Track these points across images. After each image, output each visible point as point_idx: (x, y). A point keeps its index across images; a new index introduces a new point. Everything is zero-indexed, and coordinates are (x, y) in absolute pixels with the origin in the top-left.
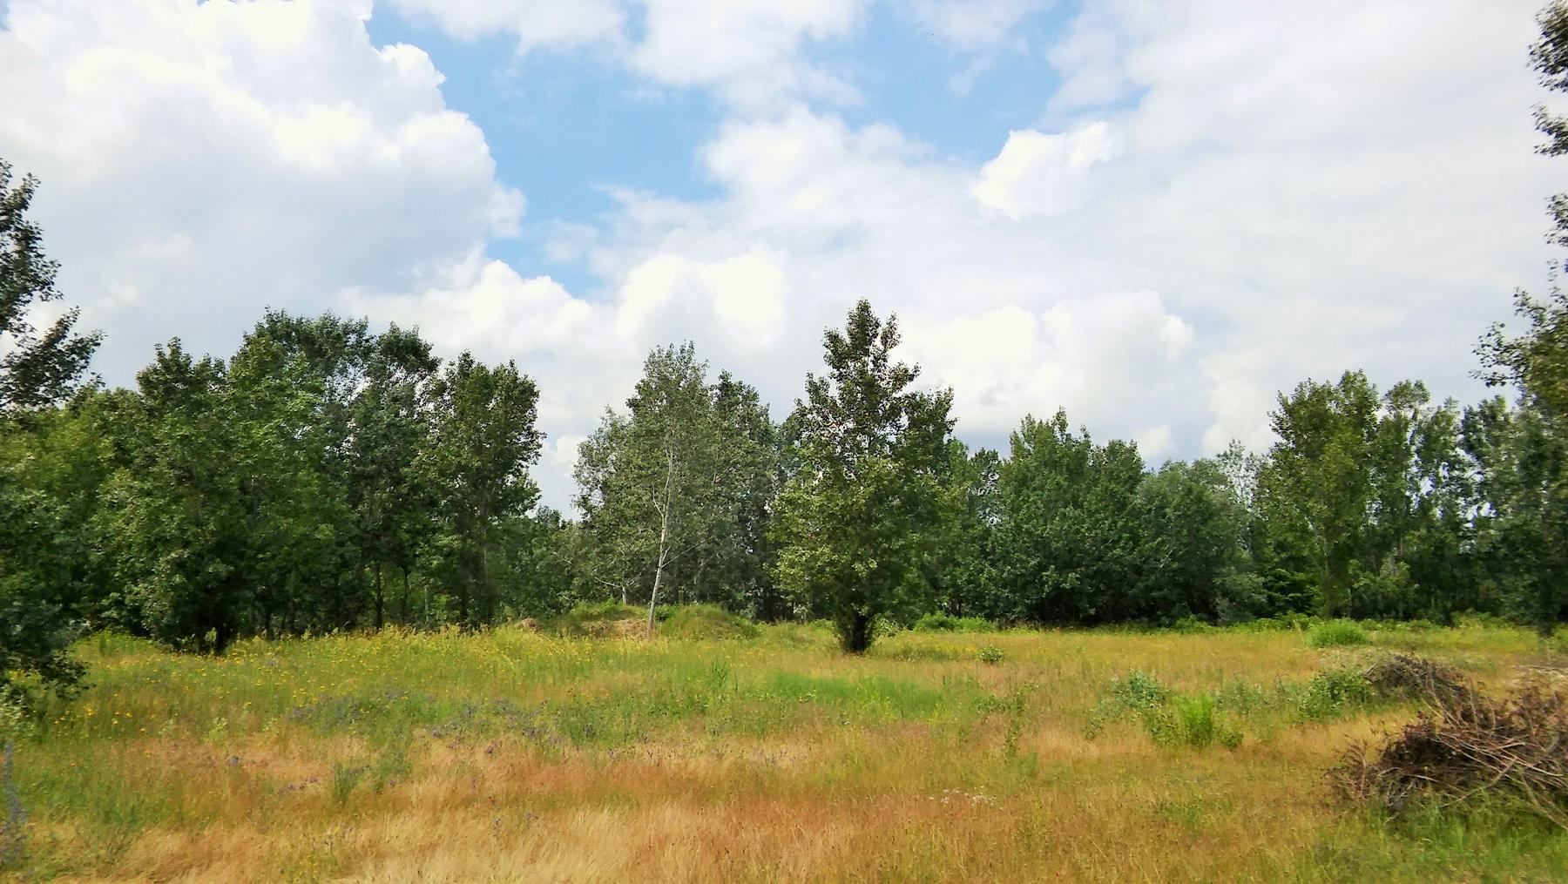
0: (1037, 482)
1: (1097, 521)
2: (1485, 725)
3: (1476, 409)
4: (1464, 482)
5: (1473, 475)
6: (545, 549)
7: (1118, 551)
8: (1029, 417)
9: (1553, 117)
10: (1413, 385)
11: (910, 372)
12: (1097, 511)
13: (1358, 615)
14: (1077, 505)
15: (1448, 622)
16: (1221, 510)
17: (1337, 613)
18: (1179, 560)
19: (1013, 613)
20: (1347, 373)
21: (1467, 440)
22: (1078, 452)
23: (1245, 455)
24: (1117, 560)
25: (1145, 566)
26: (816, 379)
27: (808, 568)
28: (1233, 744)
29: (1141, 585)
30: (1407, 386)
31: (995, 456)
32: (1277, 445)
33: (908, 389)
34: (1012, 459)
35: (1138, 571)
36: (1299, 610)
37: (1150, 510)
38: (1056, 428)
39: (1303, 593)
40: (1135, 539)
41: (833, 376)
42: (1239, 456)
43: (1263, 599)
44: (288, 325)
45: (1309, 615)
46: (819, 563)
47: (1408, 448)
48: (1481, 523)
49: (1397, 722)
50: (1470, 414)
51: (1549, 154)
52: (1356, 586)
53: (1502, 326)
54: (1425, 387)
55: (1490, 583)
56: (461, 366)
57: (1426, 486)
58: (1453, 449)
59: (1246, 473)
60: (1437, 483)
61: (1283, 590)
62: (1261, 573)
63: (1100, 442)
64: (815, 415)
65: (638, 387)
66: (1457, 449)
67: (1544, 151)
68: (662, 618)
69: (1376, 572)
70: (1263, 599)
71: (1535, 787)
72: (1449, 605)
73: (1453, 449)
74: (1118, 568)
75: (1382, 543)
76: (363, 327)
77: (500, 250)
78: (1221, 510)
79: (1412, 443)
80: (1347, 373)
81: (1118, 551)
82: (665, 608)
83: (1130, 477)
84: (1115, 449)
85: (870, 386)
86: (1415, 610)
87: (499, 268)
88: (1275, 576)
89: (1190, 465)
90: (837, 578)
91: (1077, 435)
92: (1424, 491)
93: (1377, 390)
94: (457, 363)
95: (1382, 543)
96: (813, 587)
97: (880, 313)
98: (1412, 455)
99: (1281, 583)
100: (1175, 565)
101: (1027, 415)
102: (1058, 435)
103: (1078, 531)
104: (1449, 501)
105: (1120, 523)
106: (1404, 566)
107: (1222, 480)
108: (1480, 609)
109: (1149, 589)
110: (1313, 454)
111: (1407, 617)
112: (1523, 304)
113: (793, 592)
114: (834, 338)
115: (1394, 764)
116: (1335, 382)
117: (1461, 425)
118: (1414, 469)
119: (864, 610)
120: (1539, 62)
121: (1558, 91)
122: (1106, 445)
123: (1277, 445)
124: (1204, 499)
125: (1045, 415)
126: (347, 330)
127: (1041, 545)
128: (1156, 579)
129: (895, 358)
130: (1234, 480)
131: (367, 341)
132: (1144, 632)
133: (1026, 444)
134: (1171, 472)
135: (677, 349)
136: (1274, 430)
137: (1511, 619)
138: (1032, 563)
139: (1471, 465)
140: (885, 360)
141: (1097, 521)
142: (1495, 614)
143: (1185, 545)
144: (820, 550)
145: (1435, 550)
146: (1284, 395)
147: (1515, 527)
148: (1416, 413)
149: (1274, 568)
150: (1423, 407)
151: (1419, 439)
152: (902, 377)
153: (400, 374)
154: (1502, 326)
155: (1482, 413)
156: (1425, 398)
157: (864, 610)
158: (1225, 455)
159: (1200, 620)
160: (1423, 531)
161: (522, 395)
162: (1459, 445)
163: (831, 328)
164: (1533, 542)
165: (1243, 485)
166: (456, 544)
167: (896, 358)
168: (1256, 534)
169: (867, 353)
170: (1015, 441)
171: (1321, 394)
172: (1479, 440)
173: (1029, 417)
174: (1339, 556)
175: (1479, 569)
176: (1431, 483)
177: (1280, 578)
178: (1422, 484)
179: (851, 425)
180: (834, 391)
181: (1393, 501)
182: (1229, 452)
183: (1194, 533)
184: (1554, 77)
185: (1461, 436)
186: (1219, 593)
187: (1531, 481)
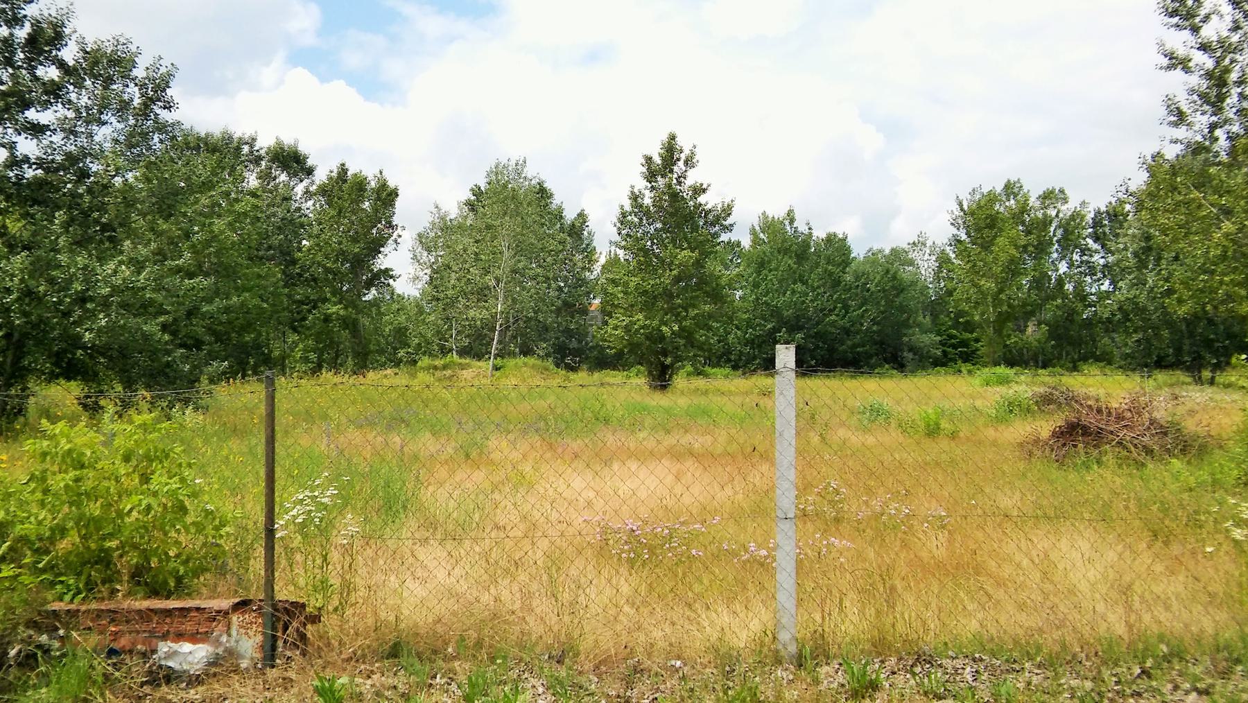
0: (773, 265)
1: (818, 294)
2: (1109, 414)
3: (1103, 209)
4: (1091, 264)
5: (1098, 259)
6: (392, 315)
7: (833, 317)
8: (764, 213)
9: (1168, 47)
10: (1057, 191)
11: (704, 186)
12: (819, 287)
13: (1011, 363)
14: (804, 283)
15: (1075, 369)
16: (910, 286)
17: (996, 364)
18: (878, 324)
19: (753, 365)
20: (1009, 181)
21: (1095, 233)
22: (804, 241)
23: (929, 243)
24: (833, 323)
25: (852, 329)
26: (636, 191)
27: (627, 329)
28: (953, 436)
29: (849, 343)
30: (1052, 192)
31: (739, 244)
32: (954, 236)
33: (702, 199)
34: (751, 246)
35: (847, 332)
36: (965, 361)
37: (858, 286)
38: (787, 222)
39: (968, 348)
40: (846, 308)
41: (646, 188)
42: (924, 244)
43: (939, 353)
44: (199, 139)
45: (973, 365)
46: (636, 327)
47: (1051, 239)
48: (1103, 296)
49: (1058, 420)
50: (1098, 213)
51: (1164, 70)
52: (1008, 343)
53: (1129, 179)
54: (1066, 192)
55: (1106, 340)
56: (339, 173)
57: (1063, 267)
58: (1084, 239)
59: (929, 258)
60: (1071, 265)
61: (954, 347)
62: (939, 334)
63: (820, 233)
64: (633, 217)
65: (472, 190)
66: (1087, 239)
67: (1161, 68)
68: (497, 368)
69: (1023, 331)
70: (939, 353)
71: (1135, 446)
72: (1076, 357)
73: (1084, 239)
74: (833, 330)
75: (1027, 312)
76: (254, 140)
77: (301, 57)
78: (910, 286)
79: (1054, 236)
80: (1009, 181)
81: (833, 317)
82: (499, 361)
83: (843, 260)
84: (830, 239)
85: (675, 196)
86: (1050, 360)
87: (301, 73)
88: (948, 336)
89: (887, 252)
90: (647, 338)
91: (803, 228)
92: (1061, 272)
93: (1030, 194)
94: (336, 171)
95: (1027, 312)
96: (630, 344)
97: (684, 143)
98: (1054, 245)
99: (953, 341)
100: (875, 328)
101: (762, 211)
102: (788, 228)
103: (803, 302)
104: (1079, 279)
105: (835, 296)
106: (1044, 328)
107: (911, 263)
108: (1098, 359)
109: (855, 346)
110: (986, 246)
111: (1044, 367)
112: (1144, 163)
113: (615, 348)
114: (649, 160)
115: (1058, 437)
116: (999, 188)
117: (1091, 221)
118: (1055, 255)
119: (669, 361)
120: (1162, 10)
121: (1173, 29)
122: (824, 236)
123: (954, 236)
124: (898, 277)
125: (777, 211)
126: (241, 142)
127: (776, 313)
128: (861, 338)
129: (693, 178)
130: (920, 262)
131: (258, 151)
132: (852, 377)
133: (762, 235)
134: (873, 257)
135: (513, 163)
136: (952, 224)
137: (1120, 367)
138: (769, 326)
139: (1096, 252)
140: (685, 178)
141: (818, 294)
142: (1110, 363)
143: (882, 313)
144: (637, 317)
145: (1068, 316)
146: (960, 198)
147: (1128, 299)
148: (1058, 212)
149: (947, 330)
150: (1064, 208)
151: (1060, 232)
152: (699, 190)
153: (283, 177)
154: (1129, 179)
155: (1107, 212)
156: (1065, 201)
157: (669, 361)
158: (914, 243)
159: (894, 368)
160: (1059, 301)
161: (387, 197)
162: (1089, 236)
163: (648, 153)
164: (1141, 311)
165: (926, 267)
166: (342, 312)
167: (693, 177)
168: (935, 308)
169: (671, 171)
170: (753, 232)
171: (991, 198)
172: (1104, 233)
173: (764, 213)
174: (1002, 319)
175: (1099, 329)
176: (1066, 265)
177: (951, 337)
178: (1060, 266)
179: (659, 225)
180: (647, 201)
181: (1040, 282)
182: (917, 241)
183: (890, 303)
184: (1171, 20)
185: (1090, 230)
186: (906, 348)
187: (1142, 265)
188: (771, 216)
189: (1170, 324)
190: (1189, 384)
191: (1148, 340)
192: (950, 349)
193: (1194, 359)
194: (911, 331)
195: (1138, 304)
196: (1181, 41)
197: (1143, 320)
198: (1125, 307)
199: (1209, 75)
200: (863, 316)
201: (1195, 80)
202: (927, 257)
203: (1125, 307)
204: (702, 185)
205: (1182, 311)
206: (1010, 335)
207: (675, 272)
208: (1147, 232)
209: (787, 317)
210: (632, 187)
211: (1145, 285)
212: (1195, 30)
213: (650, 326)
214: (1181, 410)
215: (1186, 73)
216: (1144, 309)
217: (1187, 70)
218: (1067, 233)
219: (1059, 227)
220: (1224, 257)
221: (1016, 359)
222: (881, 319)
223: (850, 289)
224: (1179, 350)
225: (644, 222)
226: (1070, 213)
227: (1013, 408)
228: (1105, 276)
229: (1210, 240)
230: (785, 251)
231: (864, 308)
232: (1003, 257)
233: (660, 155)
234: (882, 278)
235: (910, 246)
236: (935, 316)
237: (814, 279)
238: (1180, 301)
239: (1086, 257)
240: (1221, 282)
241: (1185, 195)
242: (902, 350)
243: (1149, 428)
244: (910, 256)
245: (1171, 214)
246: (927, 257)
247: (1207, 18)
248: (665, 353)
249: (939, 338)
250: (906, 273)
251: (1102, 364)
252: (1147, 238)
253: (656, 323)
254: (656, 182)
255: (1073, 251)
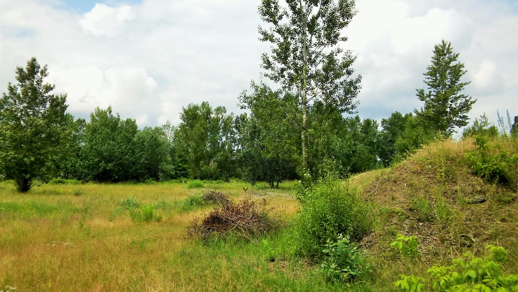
1: (121, 146)
5: (237, 136)
7: (127, 157)
9: (263, 29)
14: (114, 140)
15: (227, 181)
20: (204, 102)
21: (236, 125)
24: (127, 160)
26: (12, 85)
28: (159, 220)
30: (220, 108)
32: (181, 123)
35: (134, 163)
36: (185, 177)
37: (139, 143)
38: (108, 113)
40: (133, 153)
42: (169, 126)
43: (174, 173)
45: (187, 178)
49: (207, 212)
50: (237, 117)
53: (246, 91)
54: (226, 108)
55: (239, 169)
57: (224, 139)
60: (227, 138)
61: (180, 171)
62: (174, 165)
63: (123, 119)
64: (10, 99)
69: (208, 165)
70: (174, 173)
71: (245, 229)
73: (232, 128)
74: (126, 162)
80: (204, 102)
81: (127, 157)
83: (133, 131)
84: (128, 122)
88: (178, 166)
89: (153, 128)
90: (17, 164)
91: (115, 115)
92: (223, 140)
99: (180, 168)
101: (97, 107)
103: (113, 149)
105: (128, 147)
108: (236, 177)
109: (137, 170)
110: (192, 127)
111: (216, 179)
114: (21, 71)
116: (200, 105)
117: (235, 121)
118: (221, 134)
121: (265, 21)
122: (125, 120)
123: (181, 123)
124: (157, 140)
125: (104, 107)
128: (140, 166)
129: (46, 81)
132: (134, 184)
133: (96, 117)
134: (147, 130)
136: (181, 118)
138: (96, 160)
139: (237, 133)
142: (240, 178)
147: (247, 152)
149: (178, 163)
150: (224, 115)
151: (223, 124)
152: (49, 88)
154: (246, 91)
156: (225, 112)
158: (165, 126)
159: (153, 180)
164: (252, 157)
165: (170, 136)
169: (34, 77)
170: (92, 116)
171: (196, 108)
177: (179, 166)
178: (223, 138)
179: (25, 105)
182: (166, 125)
183: (153, 151)
187: (253, 139)
188: (101, 109)
189: (262, 162)
190: (269, 188)
191: (254, 169)
192: (178, 172)
193: (271, 178)
194: (162, 164)
195: (251, 154)
196: (269, 27)
197: (253, 161)
198: (246, 156)
199: (281, 45)
200: (141, 157)
201: (276, 46)
202: (170, 132)
203: (246, 156)
204: (50, 86)
205: (269, 156)
206: (203, 166)
207: (33, 130)
208: (255, 125)
209: (105, 156)
210: (10, 84)
211: (253, 147)
212: (275, 23)
213: (18, 157)
214: (268, 207)
215: (272, 42)
216: (253, 157)
217: (272, 41)
218: (226, 125)
219: (222, 122)
220: (287, 130)
221: (205, 177)
222: (149, 158)
223: (136, 144)
224: (265, 174)
225: (17, 103)
226: (227, 117)
227: (194, 203)
228: (239, 143)
229: (281, 123)
230: (106, 125)
231: (142, 153)
232: (198, 133)
233: (27, 69)
234: (150, 139)
235: (163, 127)
236: (172, 156)
237: (119, 139)
238: (268, 152)
239: (233, 135)
240: (286, 143)
241: (271, 100)
242: (158, 172)
243: (252, 218)
244: (163, 131)
245: (264, 109)
246: (170, 132)
247: (281, 18)
248: (26, 172)
249: (174, 167)
250: (161, 139)
251: (238, 179)
252: (255, 127)
253: (21, 156)
254: (25, 82)
255: (228, 132)
